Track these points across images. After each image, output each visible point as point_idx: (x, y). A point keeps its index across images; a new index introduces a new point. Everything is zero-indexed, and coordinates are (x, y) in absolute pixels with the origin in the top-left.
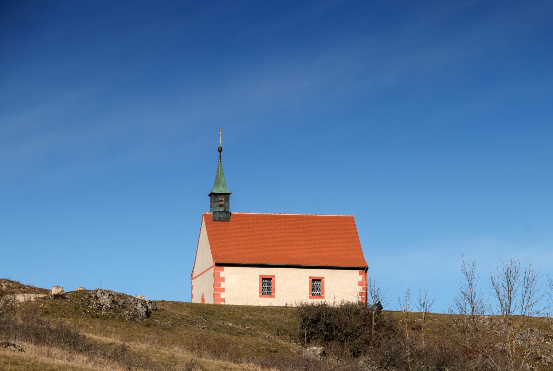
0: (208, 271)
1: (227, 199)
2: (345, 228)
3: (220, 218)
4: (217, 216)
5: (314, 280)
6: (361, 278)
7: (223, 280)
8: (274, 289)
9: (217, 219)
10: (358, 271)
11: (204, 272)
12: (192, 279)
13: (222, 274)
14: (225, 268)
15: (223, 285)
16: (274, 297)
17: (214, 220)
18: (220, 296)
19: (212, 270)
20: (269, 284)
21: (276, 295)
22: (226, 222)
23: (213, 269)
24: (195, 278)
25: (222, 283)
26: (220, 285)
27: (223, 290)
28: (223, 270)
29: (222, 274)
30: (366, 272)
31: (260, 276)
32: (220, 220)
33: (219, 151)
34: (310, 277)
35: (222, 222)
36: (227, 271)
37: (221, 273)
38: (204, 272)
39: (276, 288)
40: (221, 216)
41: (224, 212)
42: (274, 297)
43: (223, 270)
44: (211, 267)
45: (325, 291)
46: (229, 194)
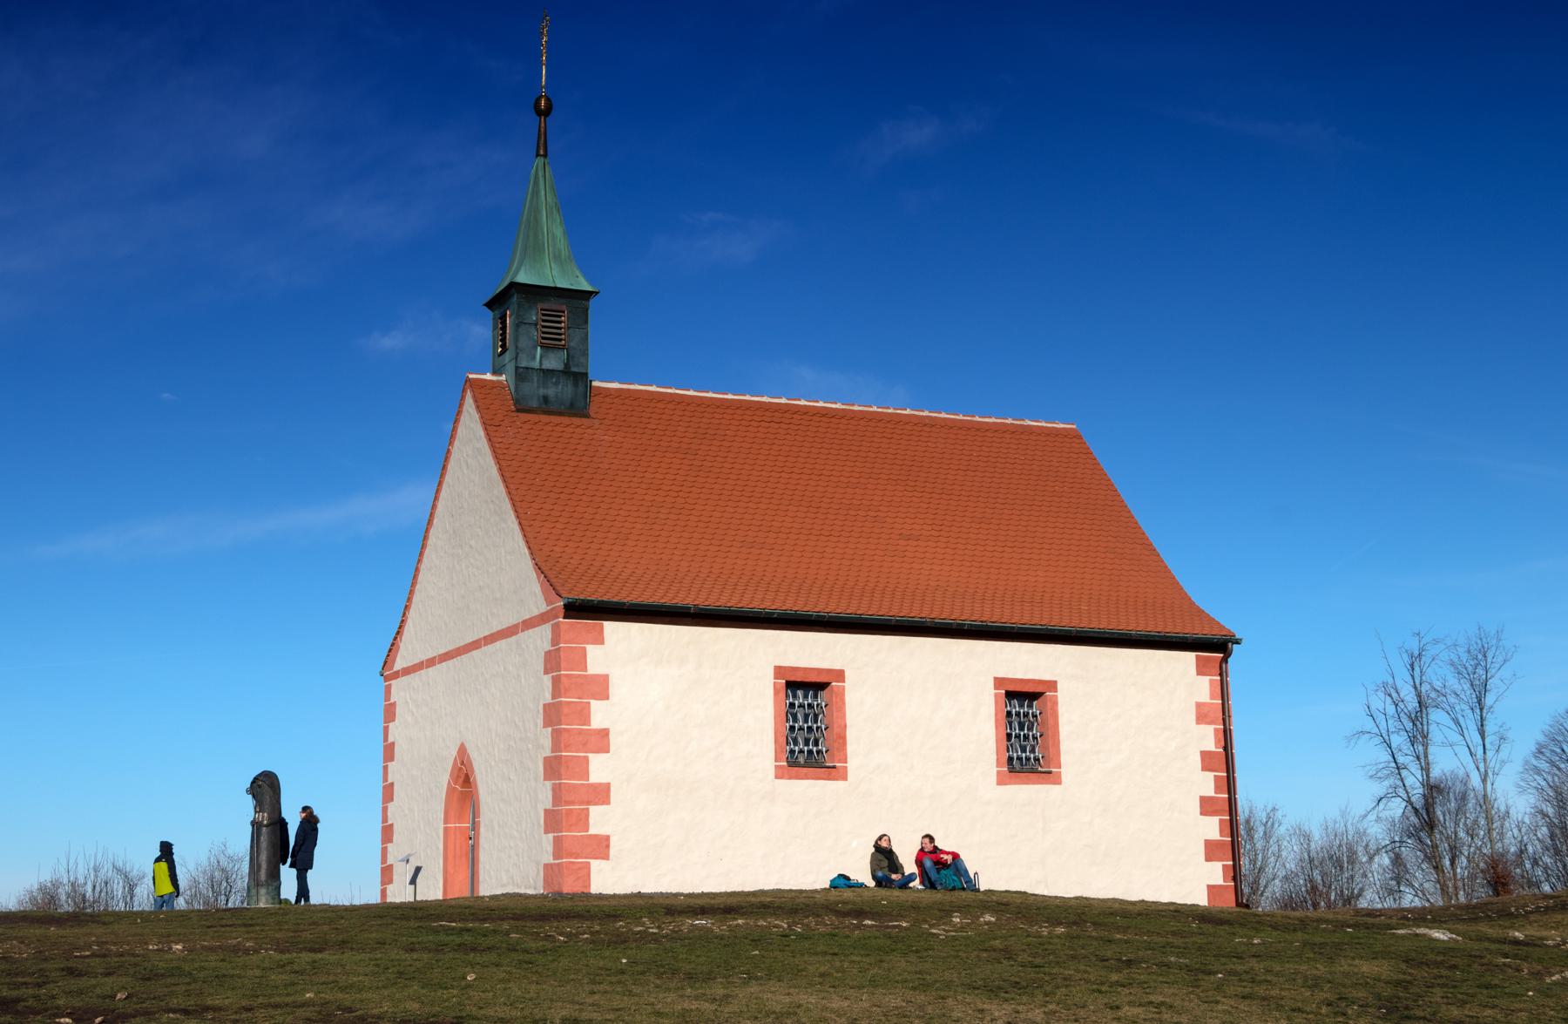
0: (502, 644)
1: (581, 318)
2: (1061, 480)
3: (546, 399)
4: (534, 389)
5: (792, 686)
6: (1203, 688)
7: (600, 687)
8: (842, 738)
9: (534, 404)
10: (1189, 658)
11: (475, 645)
12: (388, 672)
13: (597, 659)
14: (611, 628)
15: (600, 715)
16: (843, 776)
17: (522, 408)
18: (586, 775)
19: (540, 639)
20: (813, 714)
21: (853, 764)
22: (577, 421)
23: (545, 630)
24: (407, 671)
25: (595, 705)
26: (584, 715)
27: (601, 741)
28: (599, 640)
29: (597, 659)
30: (1225, 660)
31: (779, 671)
32: (546, 407)
33: (539, 113)
34: (999, 682)
35: (555, 419)
36: (621, 648)
37: (592, 650)
38: (475, 645)
39: (851, 735)
40: (551, 392)
41: (567, 372)
42: (843, 776)
43: (599, 640)
44: (528, 624)
45: (1064, 747)
46: (587, 295)
